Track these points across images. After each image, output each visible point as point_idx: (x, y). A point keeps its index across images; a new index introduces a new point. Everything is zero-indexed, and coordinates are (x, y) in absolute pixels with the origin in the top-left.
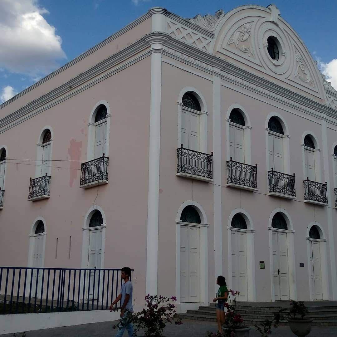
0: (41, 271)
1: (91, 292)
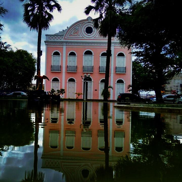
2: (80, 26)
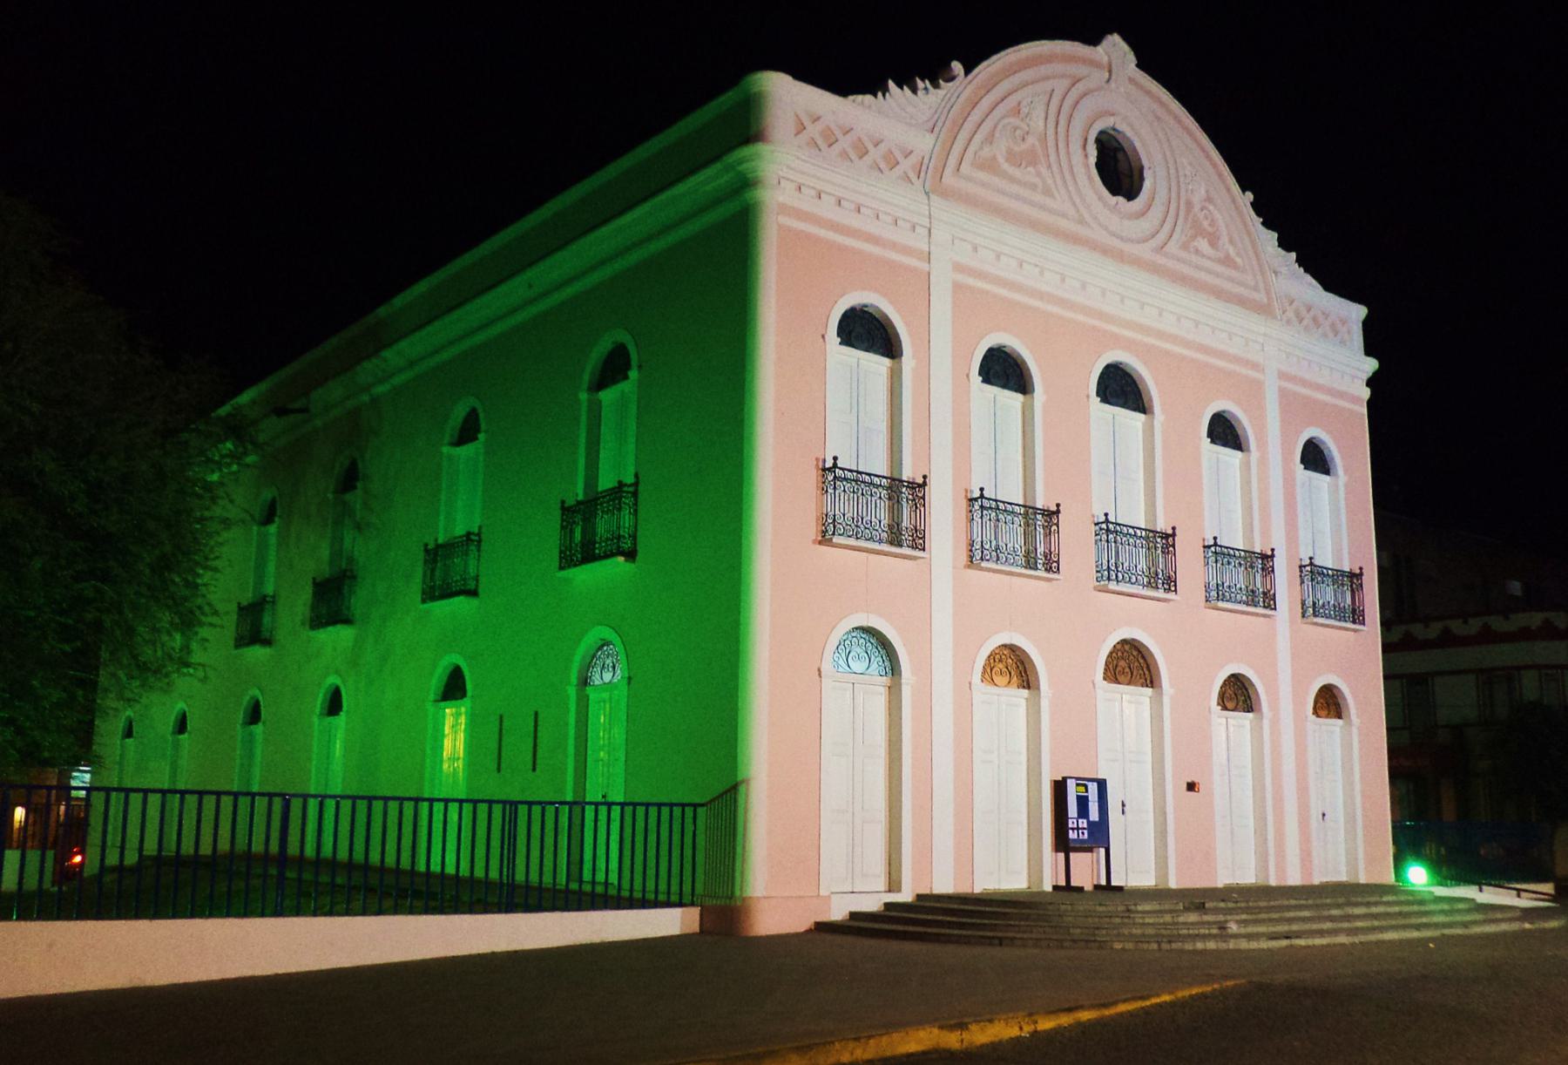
0: (454, 807)
1: (601, 864)
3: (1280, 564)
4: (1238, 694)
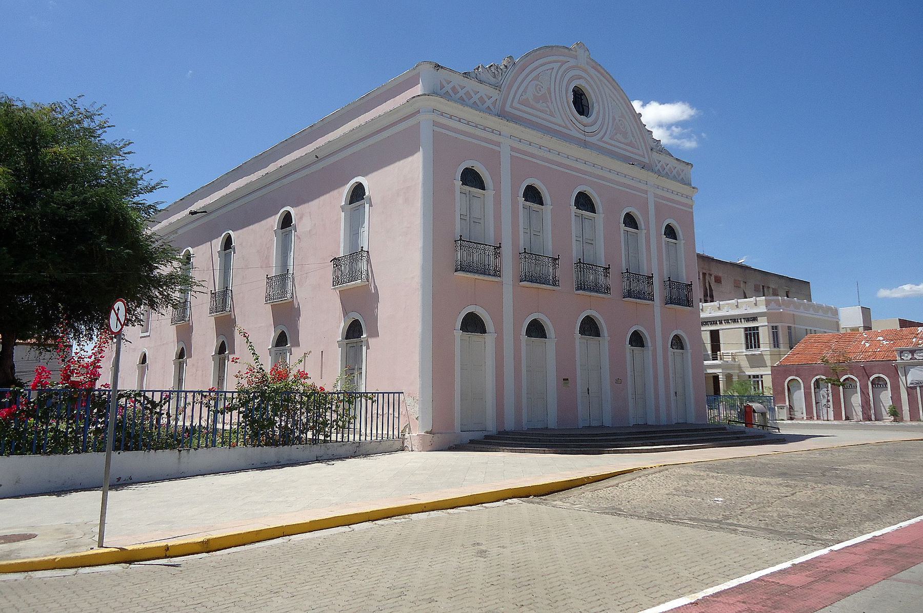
2: (555, 71)
3: (656, 280)
4: (637, 340)
